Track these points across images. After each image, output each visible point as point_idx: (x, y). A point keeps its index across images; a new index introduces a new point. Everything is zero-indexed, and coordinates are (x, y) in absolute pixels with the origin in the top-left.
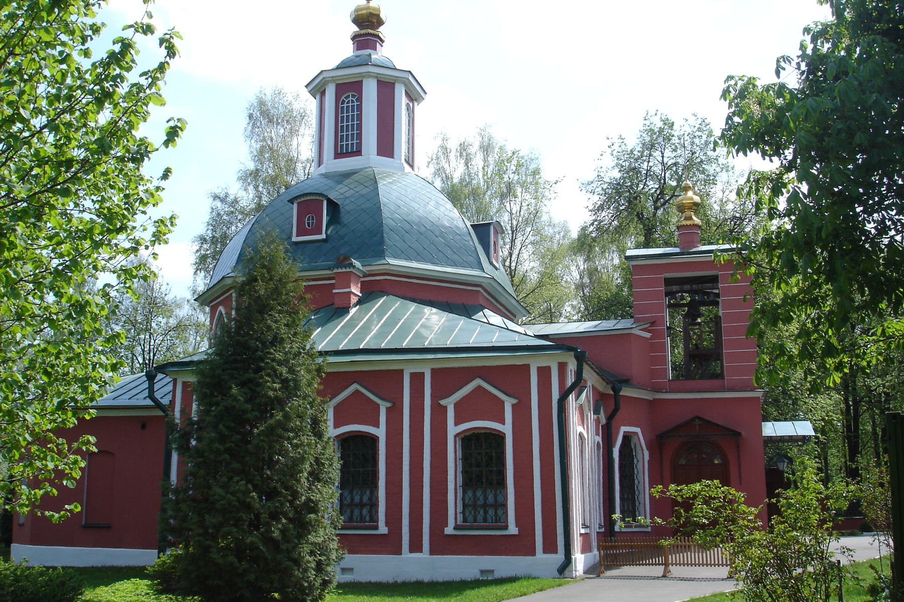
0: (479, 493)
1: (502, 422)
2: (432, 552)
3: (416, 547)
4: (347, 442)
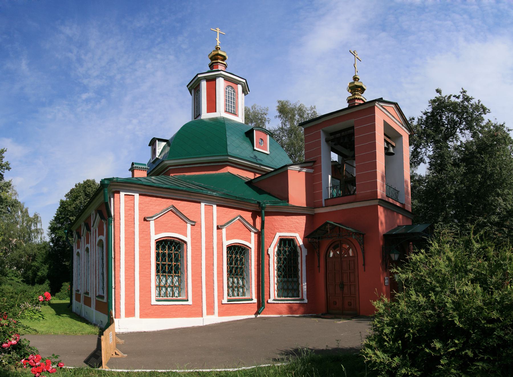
0: (235, 280)
1: (250, 242)
2: (142, 316)
3: (211, 311)
4: (232, 249)
